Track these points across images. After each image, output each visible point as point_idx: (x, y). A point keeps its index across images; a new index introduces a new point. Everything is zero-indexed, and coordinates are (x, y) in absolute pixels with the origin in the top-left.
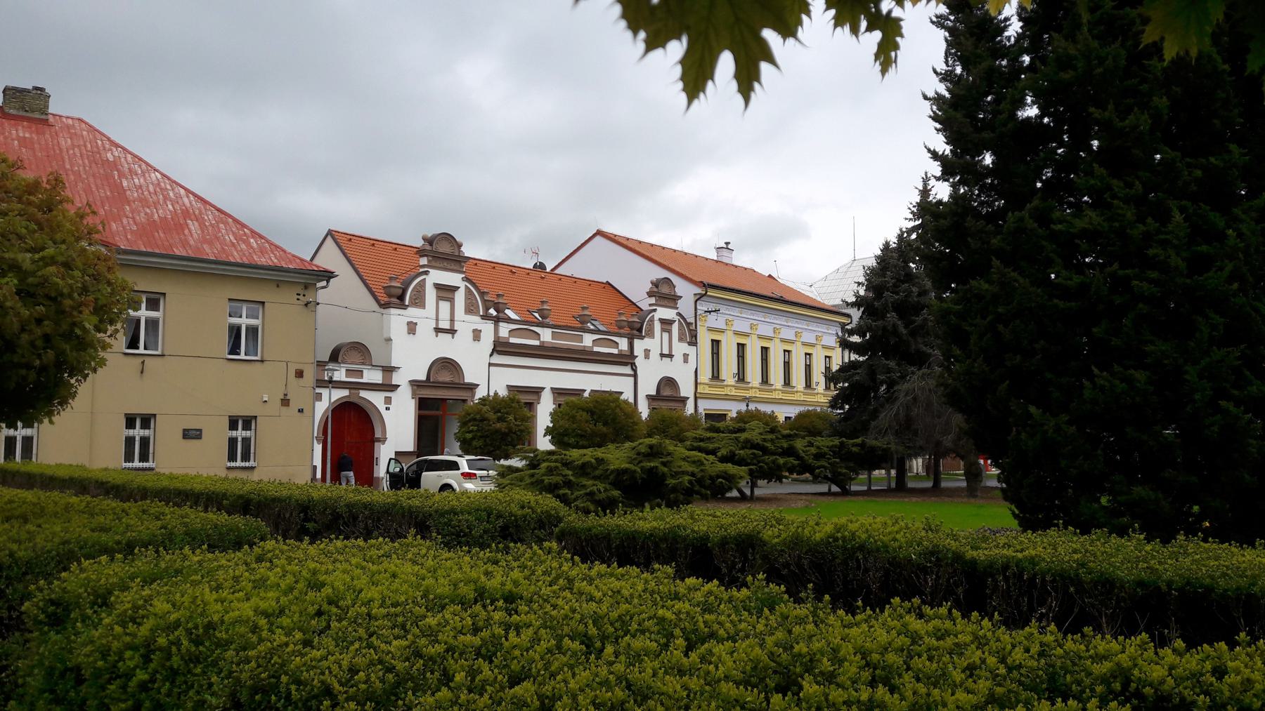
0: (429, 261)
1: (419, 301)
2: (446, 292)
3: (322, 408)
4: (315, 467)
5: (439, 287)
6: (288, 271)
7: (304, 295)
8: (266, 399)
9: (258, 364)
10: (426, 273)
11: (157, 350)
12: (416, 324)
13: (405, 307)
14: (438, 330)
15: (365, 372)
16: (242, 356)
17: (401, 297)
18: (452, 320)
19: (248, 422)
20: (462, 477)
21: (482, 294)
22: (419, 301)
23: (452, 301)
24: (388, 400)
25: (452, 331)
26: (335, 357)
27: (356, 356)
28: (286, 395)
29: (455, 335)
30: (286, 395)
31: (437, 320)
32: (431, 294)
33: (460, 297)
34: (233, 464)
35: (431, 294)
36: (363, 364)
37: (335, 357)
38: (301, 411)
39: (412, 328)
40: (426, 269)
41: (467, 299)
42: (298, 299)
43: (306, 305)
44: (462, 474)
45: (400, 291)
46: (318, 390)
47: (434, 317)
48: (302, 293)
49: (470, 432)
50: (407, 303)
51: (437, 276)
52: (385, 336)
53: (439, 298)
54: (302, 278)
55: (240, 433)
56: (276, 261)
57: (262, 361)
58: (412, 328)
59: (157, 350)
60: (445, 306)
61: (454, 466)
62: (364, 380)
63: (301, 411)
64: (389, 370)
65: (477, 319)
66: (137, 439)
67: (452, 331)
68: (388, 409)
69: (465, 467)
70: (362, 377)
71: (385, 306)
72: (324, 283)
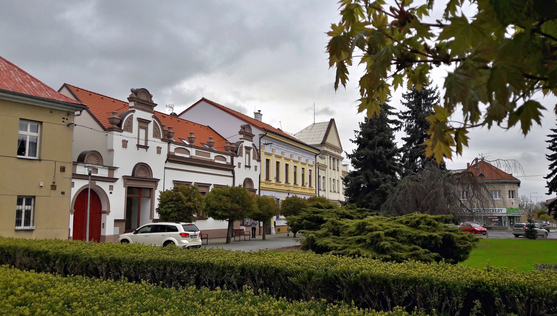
0: (135, 104)
1: (129, 128)
2: (143, 123)
3: (74, 191)
4: (70, 229)
5: (140, 120)
6: (59, 103)
7: (67, 119)
8: (42, 185)
9: (38, 162)
10: (134, 111)
11: (35, 156)
12: (127, 141)
13: (121, 131)
14: (139, 146)
15: (99, 170)
16: (26, 156)
17: (119, 125)
18: (146, 140)
19: (29, 200)
20: (180, 236)
21: (162, 126)
22: (129, 128)
23: (146, 129)
24: (111, 188)
25: (146, 147)
26: (81, 159)
27: (93, 159)
28: (54, 183)
29: (148, 150)
30: (54, 183)
31: (138, 139)
32: (135, 124)
33: (151, 127)
34: (19, 228)
35: (135, 124)
36: (98, 164)
37: (81, 159)
38: (63, 193)
39: (125, 144)
40: (133, 109)
41: (154, 128)
42: (63, 122)
43: (68, 125)
44: (181, 234)
45: (119, 121)
46: (73, 180)
47: (137, 137)
48: (66, 117)
49: (170, 208)
50: (123, 129)
51: (139, 114)
52: (109, 148)
53: (140, 127)
54: (66, 108)
55: (24, 207)
56: (50, 96)
57: (40, 160)
58: (125, 144)
59: (35, 156)
60: (142, 132)
61: (175, 229)
62: (98, 175)
63: (63, 193)
64: (112, 169)
65: (159, 140)
66: (24, 211)
67: (146, 147)
68: (111, 193)
69: (181, 230)
70: (97, 173)
71: (111, 129)
72: (78, 113)
